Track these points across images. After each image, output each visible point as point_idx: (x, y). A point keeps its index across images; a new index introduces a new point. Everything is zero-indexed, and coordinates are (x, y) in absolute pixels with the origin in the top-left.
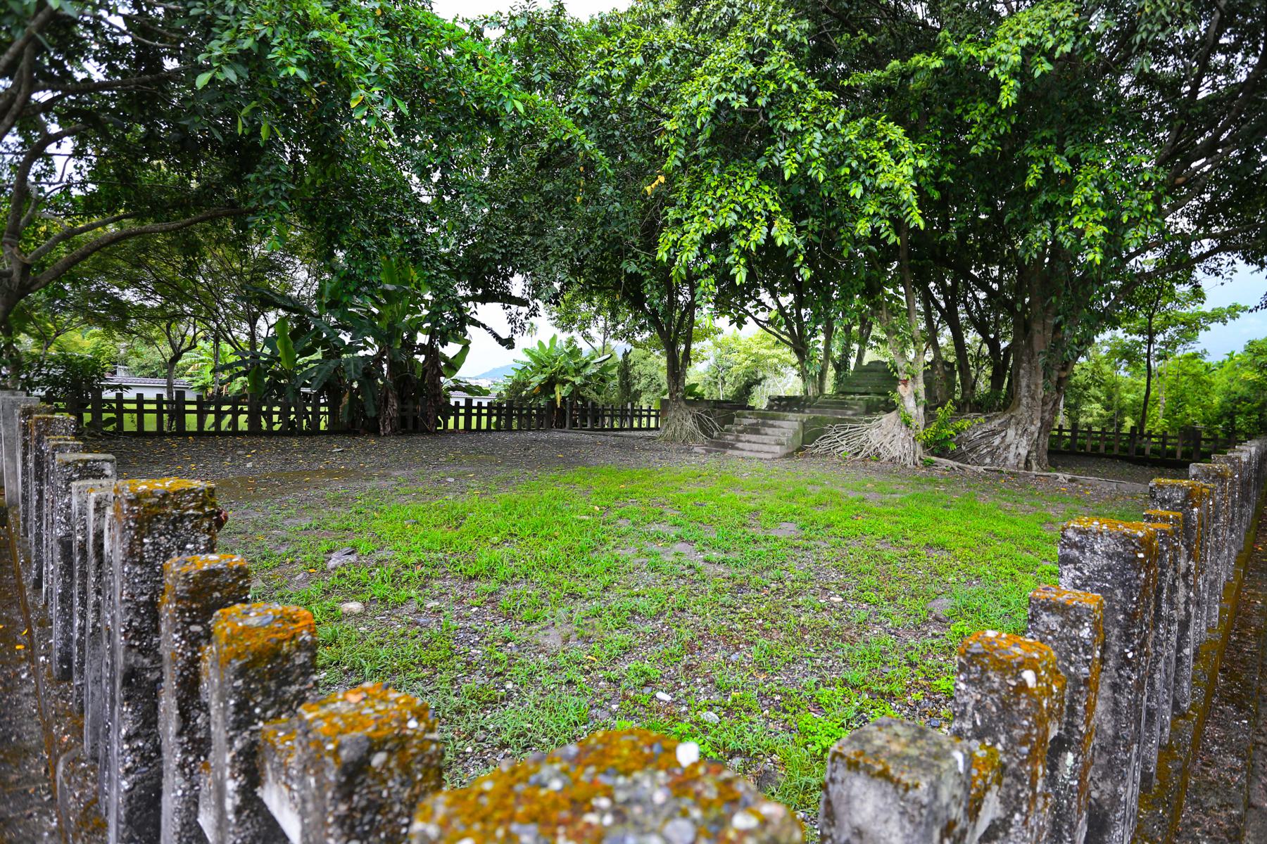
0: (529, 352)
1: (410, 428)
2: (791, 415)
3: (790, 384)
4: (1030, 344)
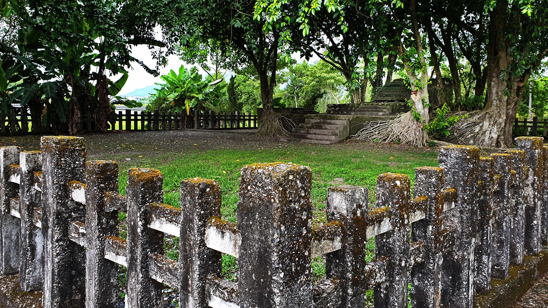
0: (165, 78)
1: (90, 129)
2: (342, 116)
3: (341, 96)
4: (498, 66)
